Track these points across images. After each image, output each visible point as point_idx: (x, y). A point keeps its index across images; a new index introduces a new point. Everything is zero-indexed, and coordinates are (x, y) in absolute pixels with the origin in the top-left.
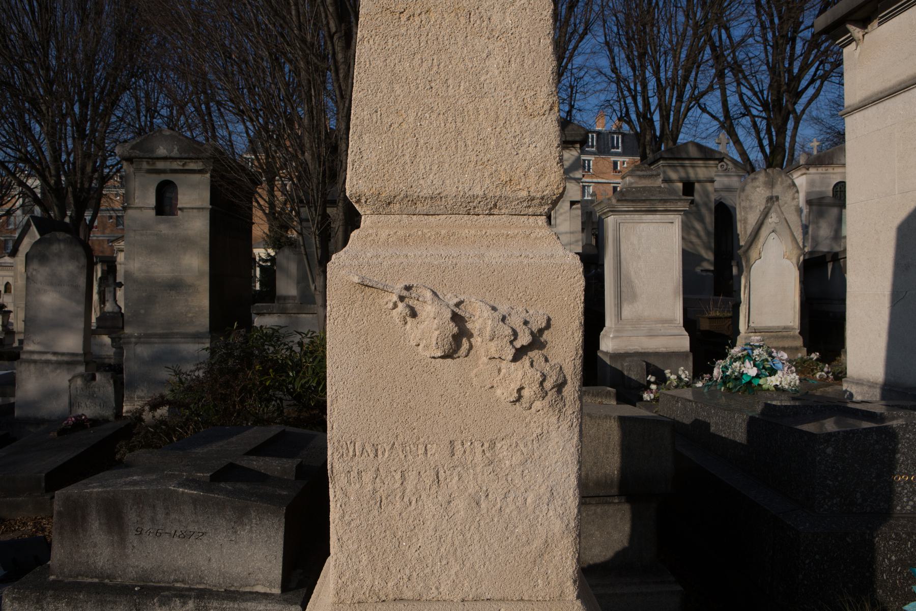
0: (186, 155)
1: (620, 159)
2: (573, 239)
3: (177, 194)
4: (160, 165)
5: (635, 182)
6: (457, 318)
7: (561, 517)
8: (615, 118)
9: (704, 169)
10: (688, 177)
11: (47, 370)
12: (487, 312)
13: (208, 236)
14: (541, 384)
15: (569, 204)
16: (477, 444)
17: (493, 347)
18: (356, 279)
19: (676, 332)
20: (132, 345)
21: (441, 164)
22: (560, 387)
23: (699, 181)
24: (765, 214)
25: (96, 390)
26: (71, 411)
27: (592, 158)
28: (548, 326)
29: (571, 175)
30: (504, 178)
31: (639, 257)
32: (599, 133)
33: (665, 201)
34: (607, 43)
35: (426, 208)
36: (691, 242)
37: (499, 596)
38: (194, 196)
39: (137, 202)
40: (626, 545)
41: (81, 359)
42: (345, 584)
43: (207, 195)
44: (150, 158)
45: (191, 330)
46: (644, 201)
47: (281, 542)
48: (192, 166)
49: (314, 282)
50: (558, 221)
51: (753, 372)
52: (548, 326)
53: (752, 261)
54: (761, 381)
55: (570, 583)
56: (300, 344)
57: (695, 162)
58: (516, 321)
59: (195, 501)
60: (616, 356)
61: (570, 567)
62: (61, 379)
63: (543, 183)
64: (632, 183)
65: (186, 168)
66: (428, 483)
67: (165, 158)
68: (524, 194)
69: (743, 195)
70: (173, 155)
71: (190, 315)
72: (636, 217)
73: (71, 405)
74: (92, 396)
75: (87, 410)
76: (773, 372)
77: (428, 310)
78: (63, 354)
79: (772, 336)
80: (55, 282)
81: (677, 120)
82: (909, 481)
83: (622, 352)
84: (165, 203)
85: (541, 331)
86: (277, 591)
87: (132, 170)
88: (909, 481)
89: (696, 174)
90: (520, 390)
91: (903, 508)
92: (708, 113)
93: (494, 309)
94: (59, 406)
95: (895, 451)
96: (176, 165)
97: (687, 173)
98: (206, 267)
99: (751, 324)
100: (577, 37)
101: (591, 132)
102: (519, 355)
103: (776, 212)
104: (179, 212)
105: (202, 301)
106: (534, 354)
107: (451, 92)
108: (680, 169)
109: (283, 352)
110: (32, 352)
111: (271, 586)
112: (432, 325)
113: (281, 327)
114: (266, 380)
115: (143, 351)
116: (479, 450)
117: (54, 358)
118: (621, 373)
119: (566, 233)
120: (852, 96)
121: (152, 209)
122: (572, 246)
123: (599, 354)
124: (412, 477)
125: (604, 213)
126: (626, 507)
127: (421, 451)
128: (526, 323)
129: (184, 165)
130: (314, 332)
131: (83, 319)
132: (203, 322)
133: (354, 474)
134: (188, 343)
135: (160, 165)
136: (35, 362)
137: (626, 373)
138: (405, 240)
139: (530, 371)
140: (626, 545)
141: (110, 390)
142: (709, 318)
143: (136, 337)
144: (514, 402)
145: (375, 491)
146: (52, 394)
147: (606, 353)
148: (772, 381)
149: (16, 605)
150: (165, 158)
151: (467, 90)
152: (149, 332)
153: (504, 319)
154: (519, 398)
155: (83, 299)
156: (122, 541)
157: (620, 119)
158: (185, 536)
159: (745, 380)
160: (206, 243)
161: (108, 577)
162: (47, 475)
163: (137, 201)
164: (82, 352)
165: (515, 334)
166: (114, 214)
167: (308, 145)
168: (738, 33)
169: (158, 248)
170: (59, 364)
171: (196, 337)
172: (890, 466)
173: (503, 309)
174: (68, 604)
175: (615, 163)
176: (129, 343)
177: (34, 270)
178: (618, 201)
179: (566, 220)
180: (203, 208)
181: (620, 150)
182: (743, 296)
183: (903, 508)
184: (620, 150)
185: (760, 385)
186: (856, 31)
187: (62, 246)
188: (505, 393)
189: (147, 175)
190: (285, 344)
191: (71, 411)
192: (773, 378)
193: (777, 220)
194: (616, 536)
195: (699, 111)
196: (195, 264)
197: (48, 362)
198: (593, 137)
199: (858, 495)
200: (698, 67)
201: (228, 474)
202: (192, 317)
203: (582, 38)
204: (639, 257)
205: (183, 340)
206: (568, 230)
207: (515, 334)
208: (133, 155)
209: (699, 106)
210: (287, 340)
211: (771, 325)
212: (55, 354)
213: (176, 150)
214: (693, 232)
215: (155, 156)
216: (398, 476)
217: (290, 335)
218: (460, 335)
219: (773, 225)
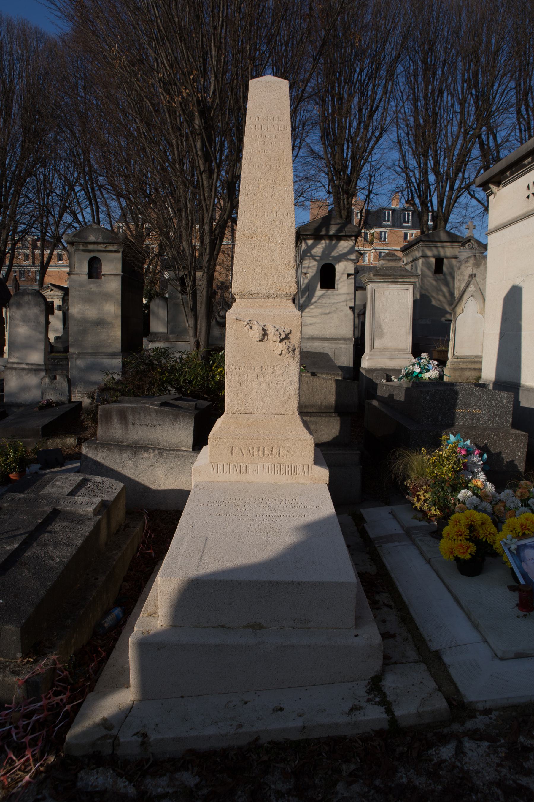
0: (107, 241)
1: (409, 232)
2: (348, 298)
3: (101, 265)
4: (91, 247)
5: (386, 264)
6: (264, 329)
7: (294, 390)
8: (404, 202)
9: (451, 249)
10: (439, 255)
11: (23, 374)
12: (273, 328)
13: (120, 292)
14: (288, 349)
15: (346, 276)
16: (269, 367)
17: (274, 338)
18: (235, 318)
19: (407, 357)
20: (74, 360)
21: (260, 284)
22: (294, 350)
23: (447, 258)
24: (468, 285)
25: (57, 385)
26: (42, 397)
27: (388, 230)
28: (291, 332)
29: (349, 257)
30: (279, 288)
31: (386, 310)
32: (394, 210)
33: (404, 276)
34: (399, 142)
35: (255, 297)
36: (439, 300)
37: (275, 413)
38: (112, 267)
39: (77, 270)
40: (338, 434)
41: (43, 367)
42: (229, 408)
43: (120, 266)
44: (84, 243)
45: (110, 350)
46: (390, 276)
47: (192, 429)
48: (111, 248)
49: (188, 322)
50: (339, 286)
51: (418, 370)
52: (291, 332)
53: (457, 314)
54: (423, 375)
55: (296, 410)
56: (181, 358)
57: (445, 244)
58: (281, 331)
59: (157, 411)
60: (370, 371)
61: (296, 405)
62: (33, 380)
63: (290, 290)
64: (384, 264)
65: (107, 249)
66: (255, 378)
67: (94, 243)
68: (285, 293)
69: (459, 272)
70: (98, 241)
71: (110, 341)
72: (385, 285)
73: (42, 394)
74: (55, 389)
75: (52, 397)
76: (428, 371)
77: (255, 327)
78: (32, 364)
79: (468, 361)
80: (25, 320)
81: (448, 205)
82: (462, 412)
83: (373, 368)
84: (94, 271)
85: (288, 334)
86: (191, 449)
87: (73, 250)
88: (462, 412)
89: (445, 252)
90: (282, 351)
91: (459, 423)
92: (476, 198)
93: (275, 327)
94: (34, 395)
95: (457, 399)
96: (101, 247)
97: (438, 251)
98: (119, 312)
99: (455, 354)
100: (374, 139)
101: (388, 209)
102: (282, 340)
103: (474, 284)
104: (103, 277)
105: (117, 333)
106: (286, 341)
107: (264, 261)
108: (434, 249)
109: (171, 362)
110: (14, 363)
111: (188, 448)
112: (257, 331)
113: (170, 348)
114: (163, 377)
115: (80, 363)
116: (270, 369)
117: (26, 367)
118: (372, 380)
119: (344, 294)
120: (492, 225)
121: (86, 274)
122: (348, 303)
123: (361, 370)
124: (249, 377)
125: (366, 283)
126: (338, 418)
127: (253, 369)
128: (284, 331)
129: (105, 247)
130: (188, 352)
131: (44, 343)
132: (118, 345)
133: (233, 375)
134: (108, 358)
135: (91, 247)
136: (15, 369)
137: (374, 380)
138: (249, 307)
139: (285, 346)
140: (338, 434)
141: (66, 385)
142: (438, 351)
143: (76, 354)
144: (280, 355)
145: (239, 380)
146: (25, 388)
147: (364, 369)
148: (426, 376)
149: (87, 449)
150: (94, 243)
151: (268, 261)
152: (84, 351)
153: (277, 330)
154: (281, 354)
155: (43, 331)
156: (126, 428)
157: (407, 202)
158: (153, 426)
159: (415, 374)
160: (119, 297)
161: (121, 442)
162: (43, 428)
163: (76, 269)
164: (43, 363)
165: (280, 334)
166: (17, 270)
167: (185, 238)
168: (501, 135)
169: (89, 299)
170: (30, 370)
171: (113, 355)
172: (454, 405)
173: (277, 327)
174: (107, 450)
175: (406, 235)
176: (72, 358)
177: (13, 312)
178: (374, 275)
179: (344, 286)
180: (117, 275)
181: (409, 224)
182: (451, 336)
183: (459, 423)
184: (409, 224)
185: (422, 377)
186: (493, 188)
187: (30, 297)
188: (277, 352)
189: (83, 253)
190: (172, 358)
191: (42, 397)
192: (428, 374)
193: (474, 289)
194: (334, 431)
195: (469, 197)
196: (112, 310)
197: (23, 369)
198: (389, 213)
199: (440, 417)
200: (466, 165)
201: (164, 404)
202: (111, 343)
203: (378, 140)
204: (386, 310)
205: (105, 357)
206: (345, 292)
207: (280, 334)
208: (74, 240)
209: (469, 193)
210: (173, 356)
211: (468, 354)
212: (27, 364)
213: (101, 238)
214: (440, 293)
215: (87, 241)
216: (246, 376)
217: (175, 353)
218: (265, 334)
219: (472, 292)
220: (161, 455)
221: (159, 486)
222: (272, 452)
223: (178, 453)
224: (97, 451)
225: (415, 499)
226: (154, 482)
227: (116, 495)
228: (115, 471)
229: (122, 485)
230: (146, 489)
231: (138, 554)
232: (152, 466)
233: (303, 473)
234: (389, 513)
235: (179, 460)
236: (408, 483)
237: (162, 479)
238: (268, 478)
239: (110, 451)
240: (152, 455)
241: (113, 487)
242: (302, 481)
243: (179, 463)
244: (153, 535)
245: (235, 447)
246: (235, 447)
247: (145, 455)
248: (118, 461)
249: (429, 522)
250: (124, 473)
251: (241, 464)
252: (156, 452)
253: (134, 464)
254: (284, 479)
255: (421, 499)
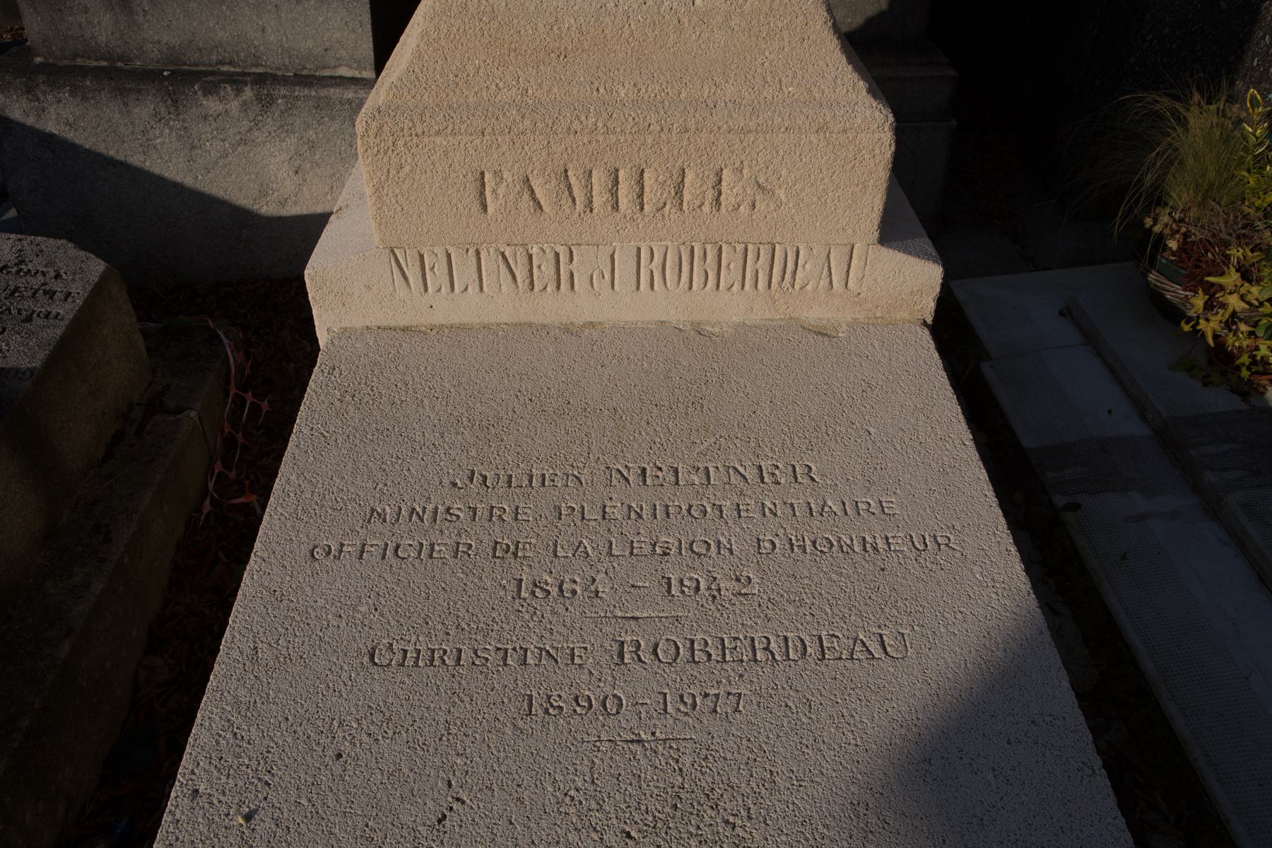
161: (120, 59)
174: (73, 93)
220: (266, 103)
221: (283, 203)
222: (679, 192)
223: (324, 92)
224: (38, 100)
225: (1199, 301)
226: (263, 193)
227: (58, 331)
228: (121, 163)
229: (97, 267)
230: (243, 219)
231: (207, 507)
232: (243, 141)
233: (824, 283)
234: (1061, 313)
235: (333, 119)
236: (1160, 223)
237: (288, 182)
238: (665, 304)
239: (84, 99)
240: (234, 106)
241: (58, 286)
242: (814, 314)
243: (335, 126)
244: (265, 406)
245: (498, 174)
246: (498, 174)
247: (212, 105)
248: (122, 130)
249: (1244, 395)
250: (157, 171)
251: (535, 251)
252: (248, 93)
253: (179, 137)
254: (731, 306)
255: (1224, 306)
